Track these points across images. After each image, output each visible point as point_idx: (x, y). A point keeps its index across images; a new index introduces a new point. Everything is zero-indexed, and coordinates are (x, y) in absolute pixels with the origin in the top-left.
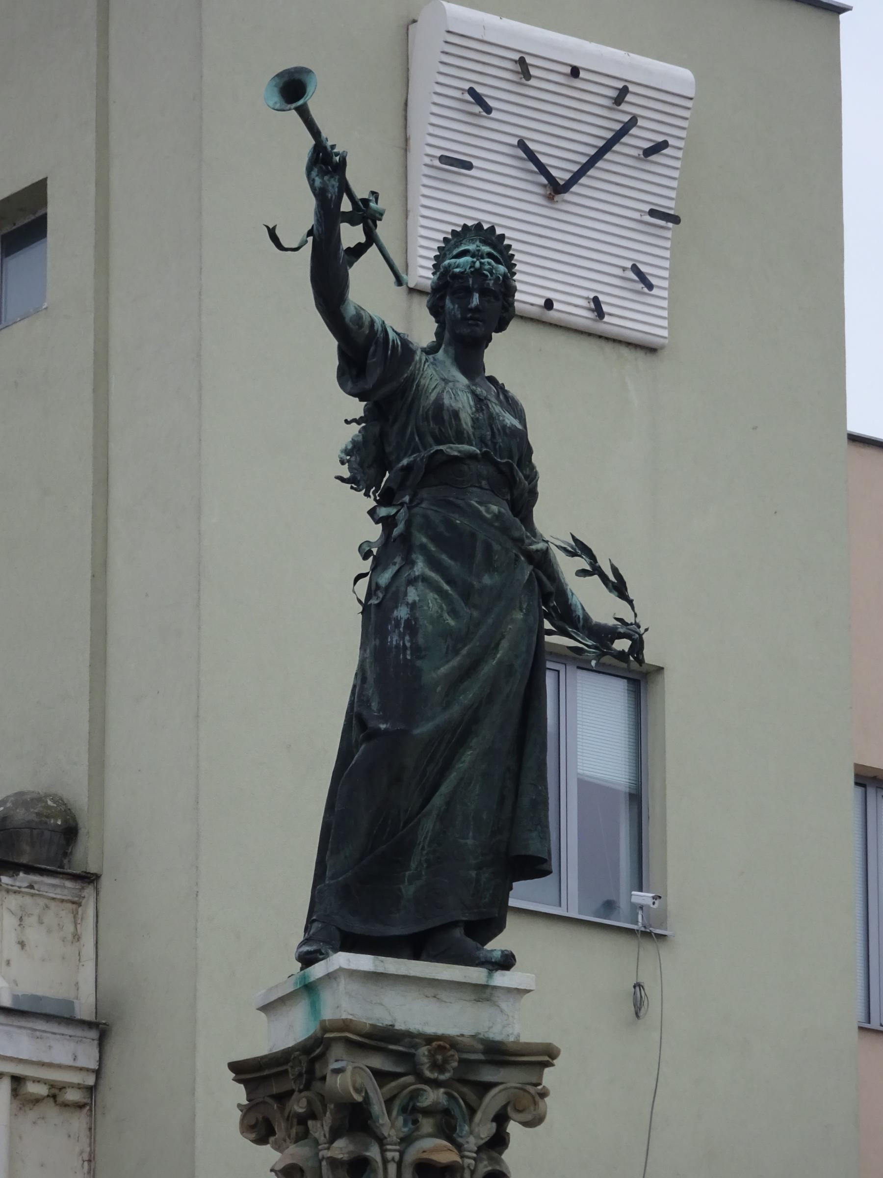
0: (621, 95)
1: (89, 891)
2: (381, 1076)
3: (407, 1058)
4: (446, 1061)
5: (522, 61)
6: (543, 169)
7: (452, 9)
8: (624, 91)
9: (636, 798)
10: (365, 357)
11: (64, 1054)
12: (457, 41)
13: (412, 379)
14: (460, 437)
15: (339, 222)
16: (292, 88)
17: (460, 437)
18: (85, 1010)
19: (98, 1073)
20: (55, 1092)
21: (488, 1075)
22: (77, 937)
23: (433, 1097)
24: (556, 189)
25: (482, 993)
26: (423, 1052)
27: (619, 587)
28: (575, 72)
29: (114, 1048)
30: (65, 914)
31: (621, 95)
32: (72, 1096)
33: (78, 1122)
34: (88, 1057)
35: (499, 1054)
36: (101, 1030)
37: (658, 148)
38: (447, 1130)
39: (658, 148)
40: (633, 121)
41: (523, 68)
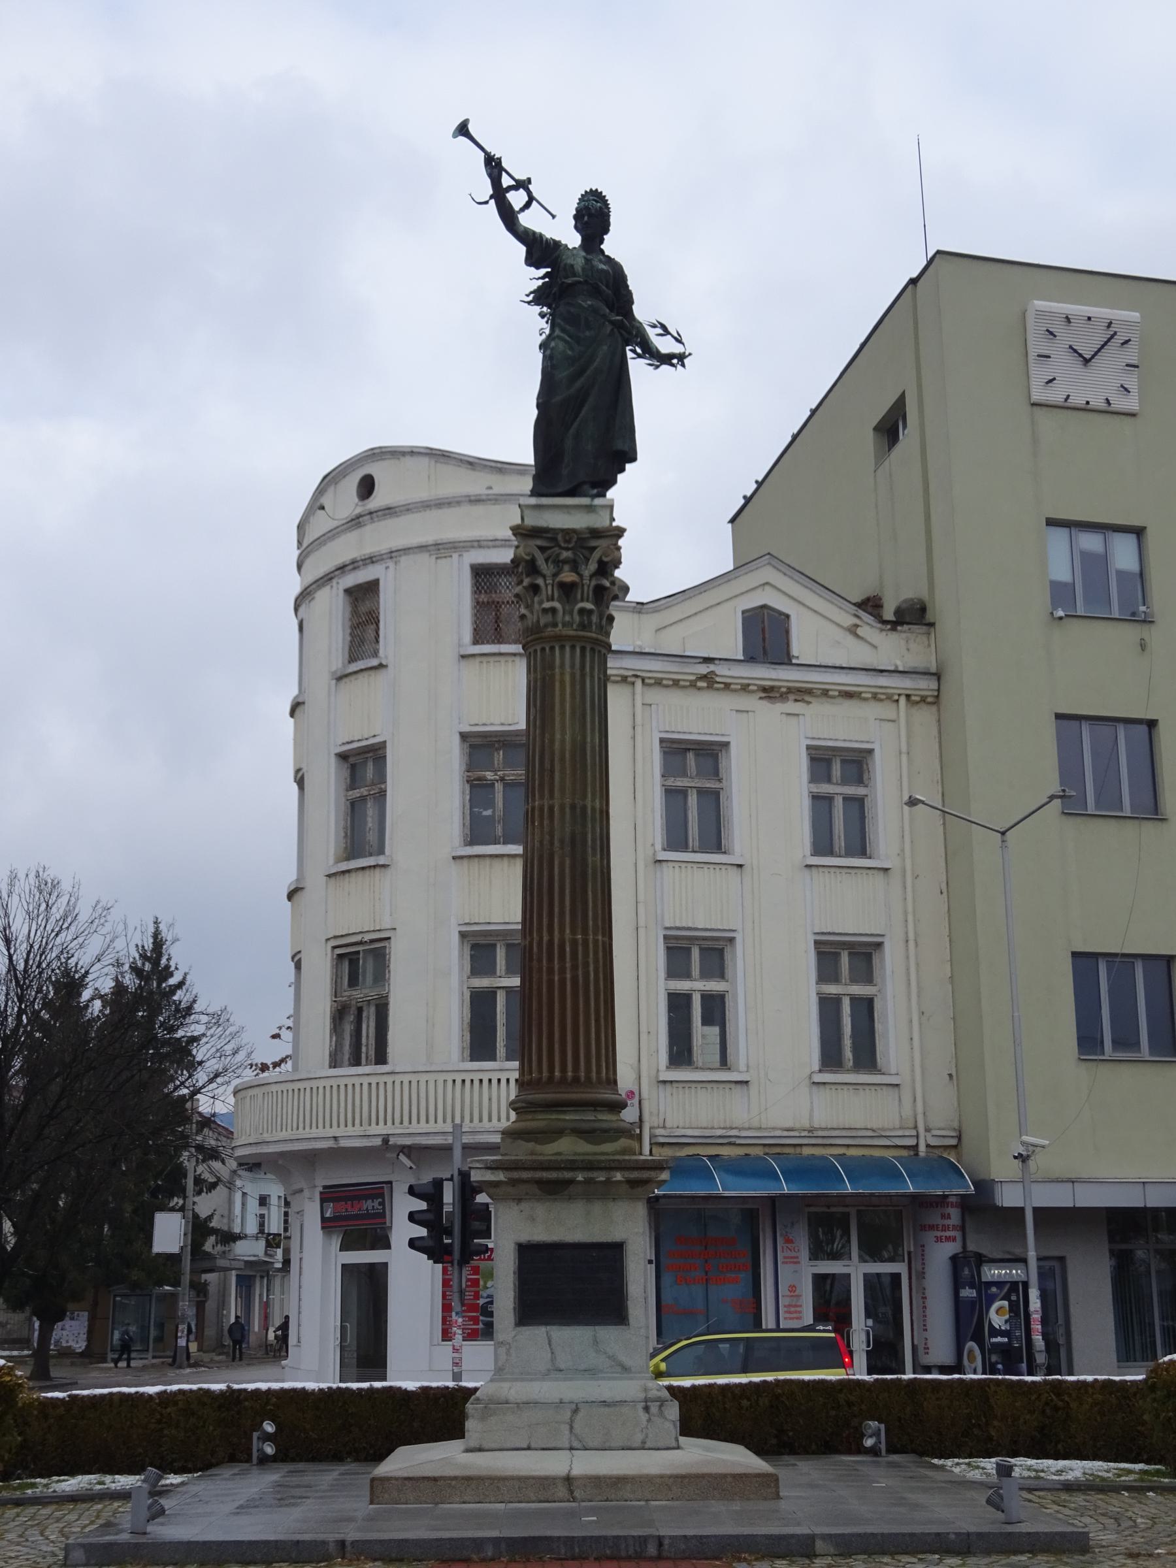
0: (1110, 325)
1: (932, 629)
2: (542, 549)
3: (554, 539)
4: (570, 539)
5: (1067, 317)
6: (1080, 355)
7: (1036, 302)
8: (1111, 323)
9: (1141, 574)
10: (539, 250)
11: (926, 685)
12: (1040, 313)
13: (558, 256)
14: (574, 275)
15: (504, 192)
16: (463, 130)
17: (574, 275)
18: (934, 670)
19: (938, 690)
20: (923, 699)
21: (593, 543)
22: (929, 645)
23: (565, 554)
24: (1087, 361)
25: (590, 509)
26: (560, 537)
27: (679, 341)
28: (1089, 318)
29: (942, 682)
30: (924, 638)
31: (1110, 325)
32: (929, 700)
33: (934, 708)
34: (934, 685)
35: (596, 533)
36: (938, 676)
37: (1126, 342)
38: (575, 568)
39: (1126, 342)
40: (1115, 333)
41: (1068, 320)
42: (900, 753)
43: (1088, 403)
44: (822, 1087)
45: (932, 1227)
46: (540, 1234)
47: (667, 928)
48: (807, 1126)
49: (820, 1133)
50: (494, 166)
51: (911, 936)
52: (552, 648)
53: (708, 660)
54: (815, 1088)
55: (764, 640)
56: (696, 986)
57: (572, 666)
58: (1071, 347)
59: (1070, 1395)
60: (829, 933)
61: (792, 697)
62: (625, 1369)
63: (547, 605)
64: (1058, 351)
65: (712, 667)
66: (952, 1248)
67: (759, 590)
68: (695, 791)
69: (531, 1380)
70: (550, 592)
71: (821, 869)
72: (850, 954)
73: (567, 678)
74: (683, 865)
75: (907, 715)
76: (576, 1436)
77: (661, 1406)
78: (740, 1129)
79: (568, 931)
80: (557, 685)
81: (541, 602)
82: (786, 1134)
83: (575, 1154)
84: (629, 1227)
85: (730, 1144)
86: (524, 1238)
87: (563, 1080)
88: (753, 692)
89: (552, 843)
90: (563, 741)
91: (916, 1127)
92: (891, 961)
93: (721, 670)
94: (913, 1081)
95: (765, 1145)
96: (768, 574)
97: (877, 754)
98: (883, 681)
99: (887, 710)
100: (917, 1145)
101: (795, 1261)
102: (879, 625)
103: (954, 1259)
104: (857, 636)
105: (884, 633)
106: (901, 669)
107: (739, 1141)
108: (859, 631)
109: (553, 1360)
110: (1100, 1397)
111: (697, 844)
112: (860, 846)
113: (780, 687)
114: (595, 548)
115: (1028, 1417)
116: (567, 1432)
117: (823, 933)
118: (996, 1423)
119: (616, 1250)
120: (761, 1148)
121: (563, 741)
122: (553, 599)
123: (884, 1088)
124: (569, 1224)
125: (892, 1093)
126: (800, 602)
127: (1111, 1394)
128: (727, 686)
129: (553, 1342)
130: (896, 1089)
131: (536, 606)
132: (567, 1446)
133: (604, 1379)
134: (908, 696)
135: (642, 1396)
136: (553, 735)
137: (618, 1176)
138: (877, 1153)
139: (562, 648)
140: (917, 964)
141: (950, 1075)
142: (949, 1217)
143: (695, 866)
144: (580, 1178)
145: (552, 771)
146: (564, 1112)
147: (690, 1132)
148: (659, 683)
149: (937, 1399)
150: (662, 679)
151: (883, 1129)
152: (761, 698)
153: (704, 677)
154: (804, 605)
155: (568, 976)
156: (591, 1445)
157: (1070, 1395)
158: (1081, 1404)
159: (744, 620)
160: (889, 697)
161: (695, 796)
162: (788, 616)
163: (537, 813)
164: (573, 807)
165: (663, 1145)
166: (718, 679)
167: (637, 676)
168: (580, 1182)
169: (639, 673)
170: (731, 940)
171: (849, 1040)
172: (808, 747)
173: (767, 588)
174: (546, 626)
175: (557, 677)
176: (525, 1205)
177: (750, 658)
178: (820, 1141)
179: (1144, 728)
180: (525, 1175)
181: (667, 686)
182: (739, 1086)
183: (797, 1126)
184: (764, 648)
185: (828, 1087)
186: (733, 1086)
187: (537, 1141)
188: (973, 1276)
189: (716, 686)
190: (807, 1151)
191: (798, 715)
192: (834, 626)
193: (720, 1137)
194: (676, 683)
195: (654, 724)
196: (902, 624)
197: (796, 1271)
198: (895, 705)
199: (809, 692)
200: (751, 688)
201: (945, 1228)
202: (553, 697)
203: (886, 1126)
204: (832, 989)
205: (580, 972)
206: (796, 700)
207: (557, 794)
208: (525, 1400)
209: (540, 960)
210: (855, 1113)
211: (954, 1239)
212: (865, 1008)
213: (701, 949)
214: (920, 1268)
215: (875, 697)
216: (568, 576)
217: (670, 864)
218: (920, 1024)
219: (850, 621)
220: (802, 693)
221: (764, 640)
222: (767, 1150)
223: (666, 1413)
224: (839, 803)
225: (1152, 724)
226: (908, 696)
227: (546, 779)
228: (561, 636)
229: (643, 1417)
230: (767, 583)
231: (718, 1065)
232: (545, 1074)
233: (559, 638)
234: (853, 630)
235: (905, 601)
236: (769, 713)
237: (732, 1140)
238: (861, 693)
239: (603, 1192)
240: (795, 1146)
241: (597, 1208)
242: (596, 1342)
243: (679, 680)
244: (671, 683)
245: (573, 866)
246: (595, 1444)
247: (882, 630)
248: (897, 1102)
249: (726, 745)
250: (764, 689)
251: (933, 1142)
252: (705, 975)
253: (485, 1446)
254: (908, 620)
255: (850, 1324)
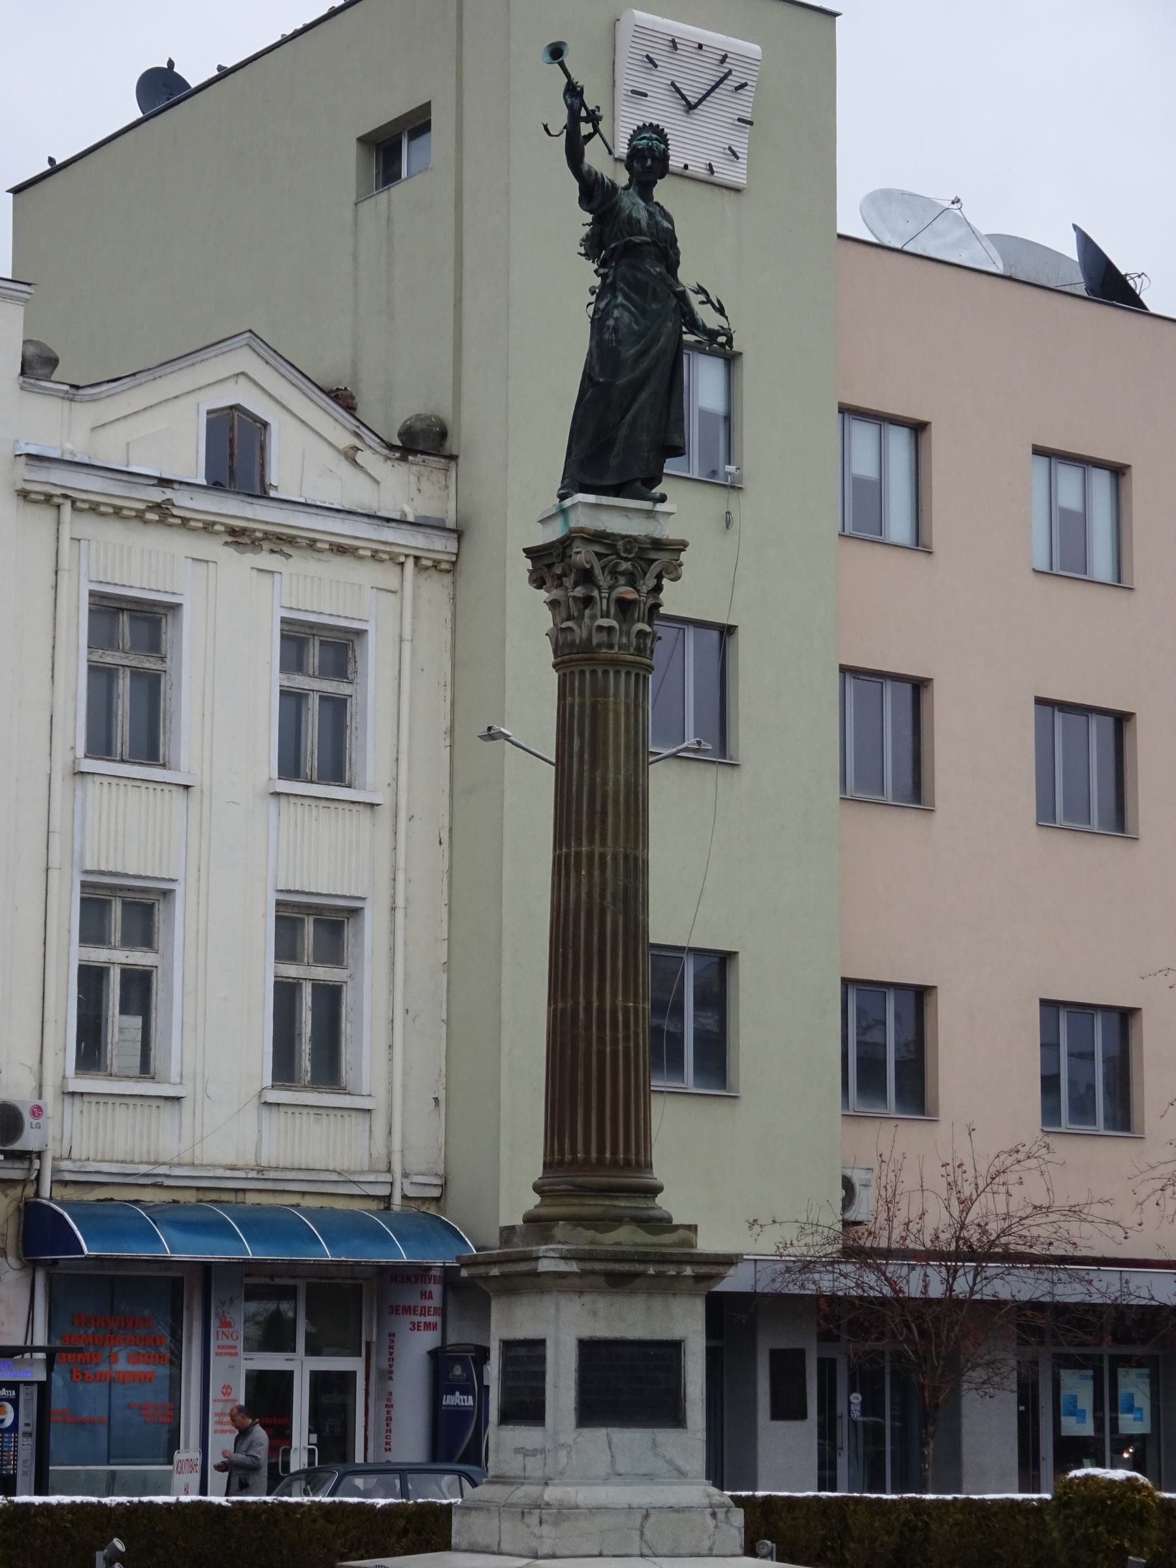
1: (453, 464)
2: (599, 556)
4: (632, 548)
5: (673, 41)
6: (683, 97)
8: (725, 57)
9: (728, 418)
10: (593, 192)
11: (442, 545)
13: (617, 202)
15: (580, 121)
16: (556, 52)
17: (641, 233)
19: (457, 555)
20: (436, 564)
22: (447, 487)
23: (625, 566)
24: (690, 107)
25: (650, 514)
27: (721, 310)
28: (700, 47)
29: (464, 543)
30: (440, 476)
32: (444, 566)
33: (447, 579)
35: (658, 545)
36: (459, 533)
40: (730, 72)
41: (674, 44)
42: (401, 640)
43: (686, 167)
44: (274, 1110)
45: (408, 1310)
46: (602, 1330)
47: (86, 872)
48: (252, 1163)
49: (272, 1175)
50: (573, 92)
51: (400, 902)
52: (606, 672)
53: (164, 482)
54: (265, 1111)
55: (232, 455)
56: (116, 957)
57: (627, 694)
58: (673, 84)
59: (929, 1515)
60: (297, 892)
61: (266, 545)
62: (682, 1474)
63: (605, 622)
64: (656, 86)
65: (169, 494)
66: (428, 1340)
67: (231, 383)
68: (128, 671)
69: (594, 1485)
70: (605, 608)
71: (292, 800)
72: (316, 921)
73: (623, 709)
74: (114, 781)
75: (416, 586)
76: (646, 1542)
77: (727, 1512)
78: (171, 1165)
79: (620, 998)
80: (611, 715)
81: (593, 618)
82: (229, 1174)
83: (636, 1245)
84: (686, 1323)
85: (155, 1185)
86: (586, 1333)
87: (615, 1162)
88: (217, 533)
89: (603, 896)
90: (616, 782)
91: (389, 1170)
92: (371, 937)
93: (182, 499)
94: (390, 1106)
95: (198, 1189)
96: (243, 359)
97: (371, 638)
98: (389, 534)
99: (386, 576)
100: (390, 1197)
101: (231, 1352)
102: (385, 452)
103: (434, 1354)
104: (354, 462)
105: (390, 463)
106: (411, 519)
107: (167, 1182)
108: (360, 457)
109: (613, 1463)
110: (960, 1517)
111: (126, 750)
112: (335, 769)
113: (254, 530)
114: (653, 561)
115: (886, 1539)
116: (638, 1539)
117: (288, 891)
118: (852, 1545)
119: (673, 1349)
120: (194, 1192)
121: (616, 782)
122: (608, 616)
123: (353, 1113)
124: (631, 1320)
125: (359, 1121)
126: (284, 407)
127: (970, 1513)
128: (185, 521)
129: (613, 1446)
130: (368, 1116)
131: (587, 620)
132: (638, 1552)
133: (663, 1484)
134: (417, 558)
135: (706, 1501)
136: (605, 772)
137: (688, 1271)
138: (339, 1204)
139: (617, 673)
140: (406, 943)
141: (436, 1099)
142: (431, 1297)
143: (130, 783)
144: (651, 1271)
145: (604, 813)
146: (617, 1198)
147: (105, 1167)
148: (94, 509)
149: (793, 1519)
150: (99, 504)
151: (354, 1173)
152: (226, 543)
153: (156, 507)
154: (284, 407)
155: (621, 1048)
156: (660, 1552)
157: (929, 1515)
158: (941, 1525)
159: (209, 422)
160: (393, 558)
161: (128, 680)
162: (265, 425)
163: (584, 861)
164: (626, 857)
165: (66, 1183)
166: (175, 512)
167: (66, 496)
168: (652, 1276)
169: (70, 493)
170: (167, 894)
171: (309, 1042)
172: (284, 621)
173: (242, 379)
174: (599, 645)
175: (611, 707)
176: (587, 1299)
177: (215, 485)
178: (269, 1186)
179: (715, 635)
180: (598, 1266)
181: (103, 514)
182: (169, 1104)
183: (240, 1163)
184: (231, 468)
185: (282, 1109)
186: (161, 1103)
187: (596, 1229)
188: (470, 1378)
189: (171, 520)
190: (251, 1199)
191: (273, 572)
192: (325, 447)
193: (145, 1175)
194: (118, 512)
195: (83, 570)
196: (415, 452)
197: (232, 1367)
198: (398, 568)
199: (291, 541)
200: (217, 527)
201: (424, 1311)
202: (606, 727)
203: (352, 1168)
204: (291, 971)
205: (632, 1044)
206: (272, 551)
207: (610, 841)
208: (595, 1505)
209: (588, 1028)
210: (319, 1148)
211: (435, 1327)
212: (330, 999)
213: (124, 904)
214: (385, 1364)
215: (375, 556)
216: (625, 591)
217: (98, 779)
218: (404, 1026)
219: (346, 440)
220: (282, 542)
221: (232, 455)
222: (201, 1195)
223: (732, 1520)
224: (314, 702)
225: (727, 631)
226: (417, 558)
227: (598, 822)
228: (617, 660)
229: (709, 1519)
230: (243, 373)
231: (136, 1071)
232: (594, 1155)
233: (615, 663)
234: (350, 456)
235: (418, 417)
236: (236, 566)
237: (159, 1180)
238: (357, 549)
239: (664, 1286)
240: (237, 1191)
241: (657, 1303)
242: (654, 1445)
243: (121, 508)
244: (111, 510)
245: (626, 927)
246: (665, 1551)
247: (387, 458)
248: (367, 1134)
249: (175, 608)
250: (232, 531)
251: (412, 1192)
252: (128, 942)
253: (558, 1552)
254: (420, 448)
255: (289, 1438)
